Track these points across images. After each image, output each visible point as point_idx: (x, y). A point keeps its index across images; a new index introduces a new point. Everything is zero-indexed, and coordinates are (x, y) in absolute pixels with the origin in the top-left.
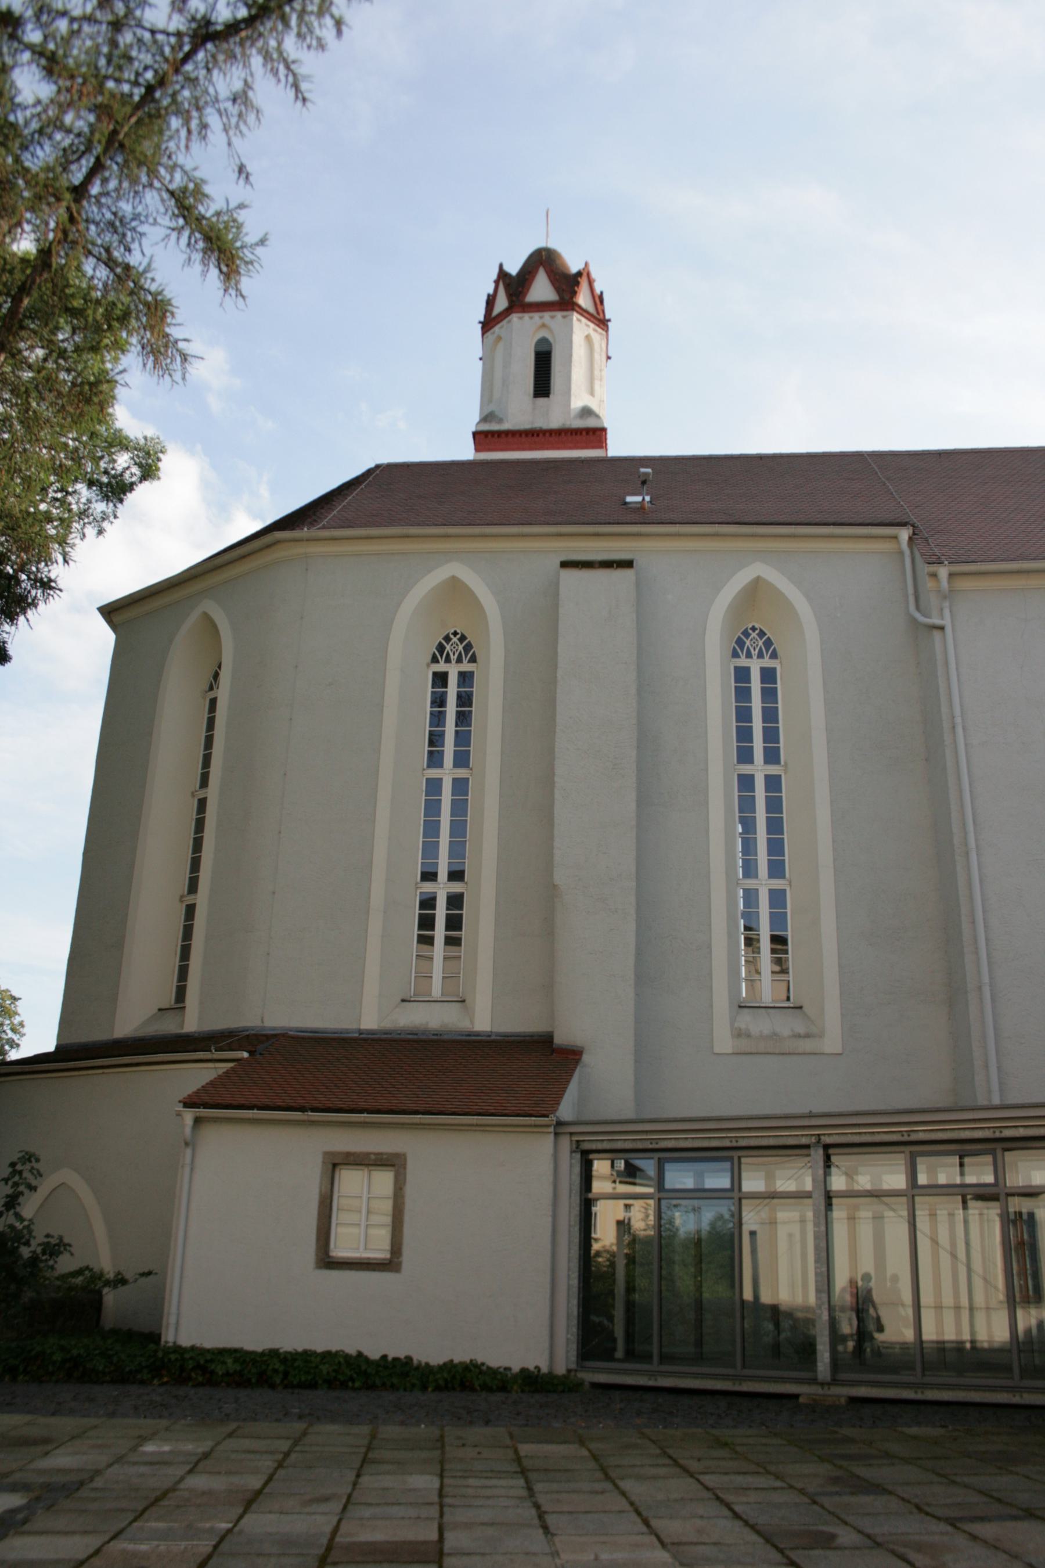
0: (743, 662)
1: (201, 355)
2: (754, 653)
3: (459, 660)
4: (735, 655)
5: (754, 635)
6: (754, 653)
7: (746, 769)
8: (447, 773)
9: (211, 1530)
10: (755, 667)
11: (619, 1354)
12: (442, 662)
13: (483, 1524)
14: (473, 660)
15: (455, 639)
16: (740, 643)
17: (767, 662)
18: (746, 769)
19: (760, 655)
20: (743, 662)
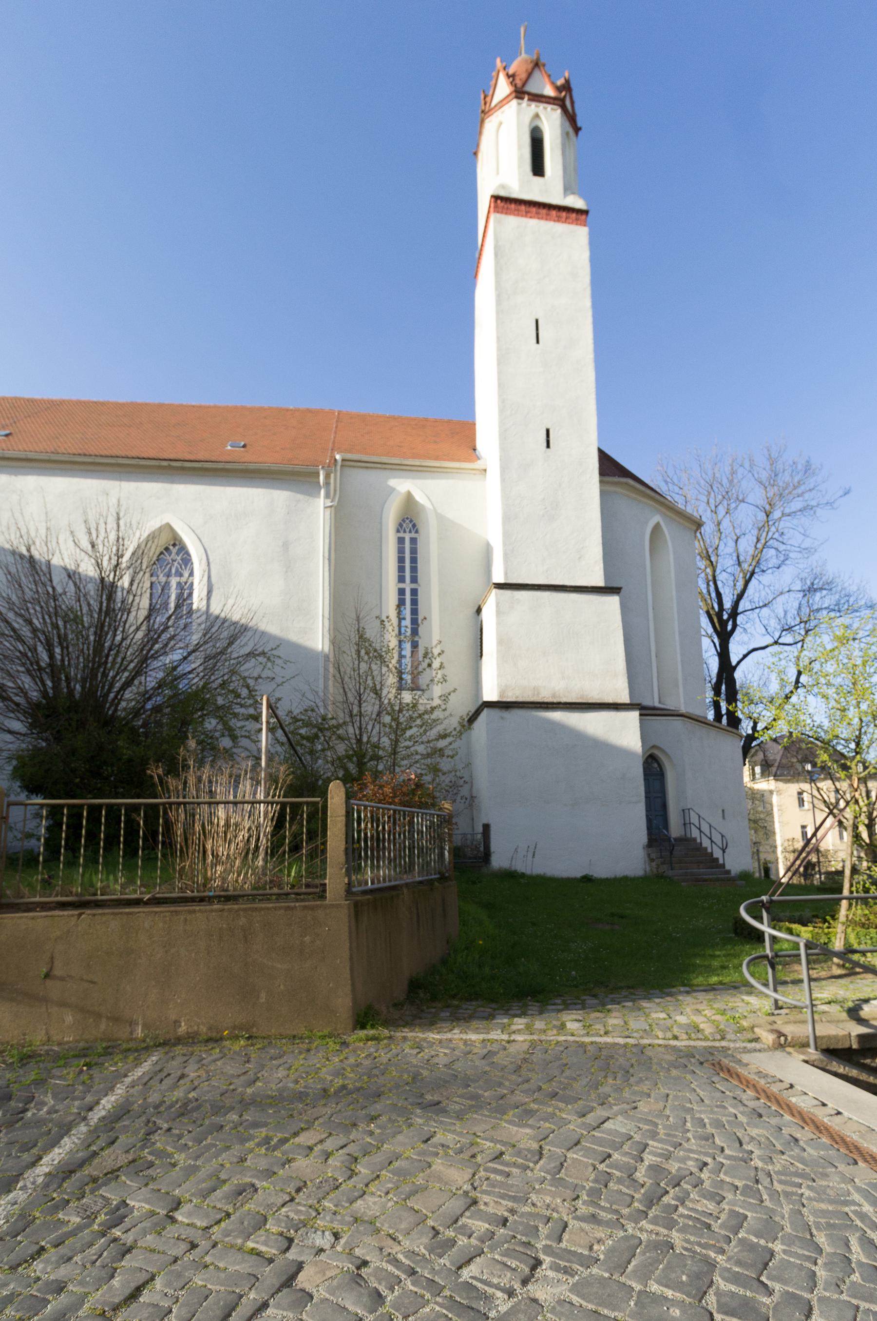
0: (401, 535)
1: (545, 432)
2: (408, 530)
3: (410, 532)
4: (398, 531)
5: (407, 521)
6: (408, 530)
7: (414, 586)
8: (408, 586)
9: (603, 1132)
10: (407, 537)
11: (810, 951)
12: (402, 532)
13: (372, 1180)
14: (417, 532)
15: (407, 521)
16: (401, 525)
17: (413, 535)
18: (414, 586)
19: (410, 532)
20: (401, 535)
